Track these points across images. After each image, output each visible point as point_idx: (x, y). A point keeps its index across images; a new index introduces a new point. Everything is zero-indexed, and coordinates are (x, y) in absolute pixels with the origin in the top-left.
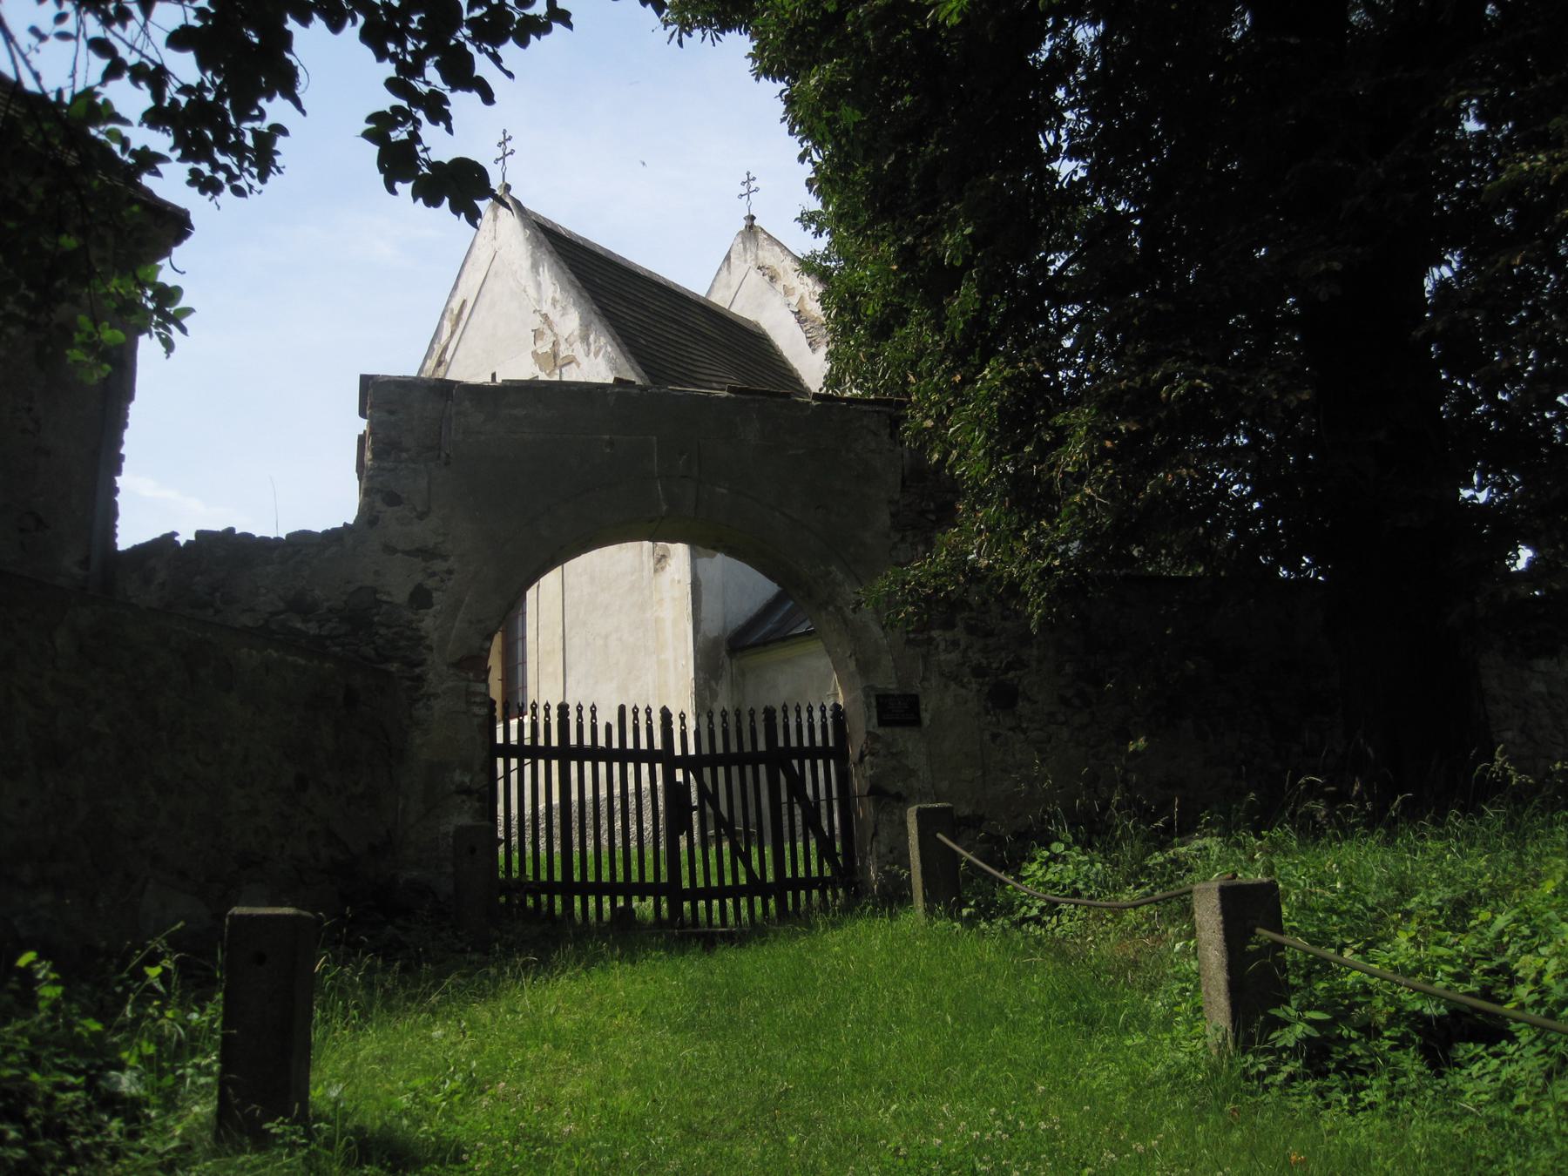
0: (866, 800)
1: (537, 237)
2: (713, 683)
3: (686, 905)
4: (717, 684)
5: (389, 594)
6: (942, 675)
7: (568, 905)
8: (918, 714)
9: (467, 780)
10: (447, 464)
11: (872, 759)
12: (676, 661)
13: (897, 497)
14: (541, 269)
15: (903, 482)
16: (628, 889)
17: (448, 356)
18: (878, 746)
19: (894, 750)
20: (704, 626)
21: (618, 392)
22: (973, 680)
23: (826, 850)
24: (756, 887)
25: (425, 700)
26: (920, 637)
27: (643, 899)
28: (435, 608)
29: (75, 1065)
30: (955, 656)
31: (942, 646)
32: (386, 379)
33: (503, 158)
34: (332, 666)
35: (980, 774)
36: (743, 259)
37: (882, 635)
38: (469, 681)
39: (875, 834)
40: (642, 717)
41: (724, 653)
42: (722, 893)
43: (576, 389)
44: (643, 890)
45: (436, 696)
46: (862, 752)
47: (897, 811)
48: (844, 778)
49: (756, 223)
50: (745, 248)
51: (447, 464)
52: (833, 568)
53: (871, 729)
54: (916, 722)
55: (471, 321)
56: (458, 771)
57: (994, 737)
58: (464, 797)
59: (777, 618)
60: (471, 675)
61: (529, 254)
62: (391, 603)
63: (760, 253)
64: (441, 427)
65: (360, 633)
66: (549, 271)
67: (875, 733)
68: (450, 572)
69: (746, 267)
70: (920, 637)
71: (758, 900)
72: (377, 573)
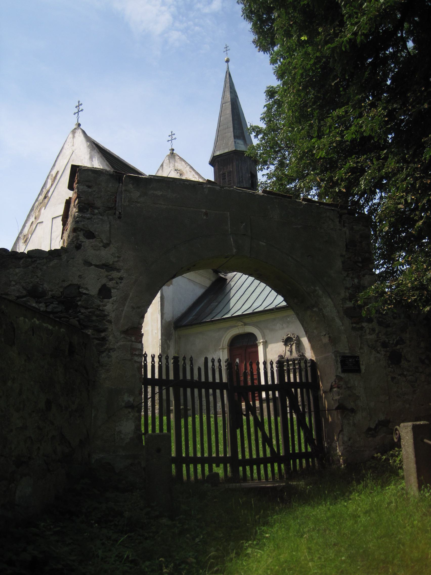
0: (335, 413)
1: (93, 146)
2: (168, 341)
3: (241, 468)
4: (170, 342)
5: (87, 289)
6: (369, 346)
7: (179, 470)
8: (359, 366)
9: (131, 399)
10: (120, 218)
11: (339, 390)
12: (152, 331)
13: (344, 253)
14: (94, 159)
15: (346, 246)
16: (210, 461)
17: (50, 194)
18: (341, 383)
19: (349, 385)
20: (165, 316)
21: (209, 187)
22: (382, 349)
23: (308, 440)
25: (107, 352)
26: (358, 326)
27: (218, 466)
28: (113, 299)
30: (373, 337)
31: (368, 331)
32: (86, 168)
33: (78, 112)
34: (64, 330)
35: (388, 398)
36: (169, 166)
37: (341, 324)
38: (132, 342)
39: (342, 431)
40: (216, 364)
41: (172, 328)
43: (188, 183)
44: (218, 461)
45: (114, 350)
46: (331, 386)
47: (351, 418)
48: (317, 399)
49: (174, 152)
50: (170, 162)
51: (120, 218)
52: (317, 288)
53: (338, 374)
54: (358, 371)
55: (61, 180)
56: (126, 394)
57: (393, 378)
58: (130, 410)
59: (194, 314)
60: (133, 338)
61: (89, 152)
62: (88, 294)
63: (176, 164)
64: (116, 197)
65: (70, 311)
66: (97, 160)
67: (340, 376)
68: (121, 278)
69: (170, 169)
70: (358, 326)
71: (276, 465)
72: (80, 276)
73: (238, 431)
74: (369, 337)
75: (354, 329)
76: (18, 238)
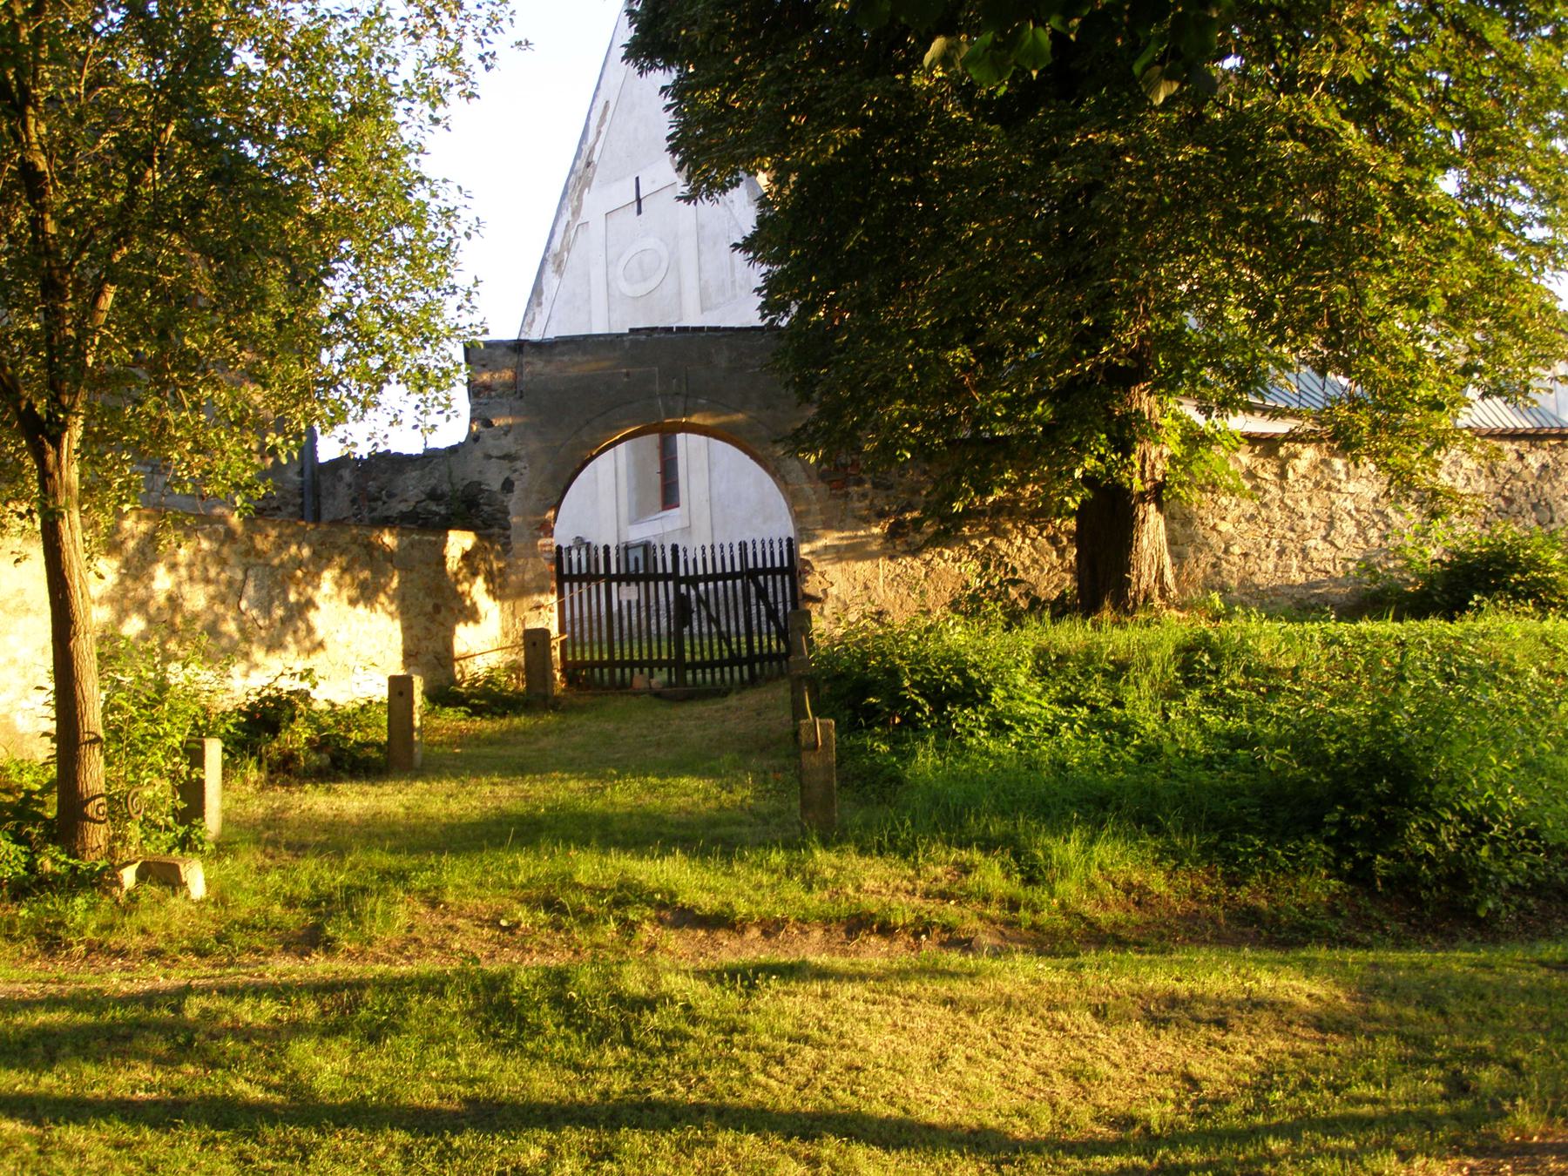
7: (612, 674)
24: (735, 660)
29: (93, 1002)
42: (712, 664)
44: (660, 664)
73: (686, 630)
74: (858, 505)
75: (835, 496)
76: (544, 261)
